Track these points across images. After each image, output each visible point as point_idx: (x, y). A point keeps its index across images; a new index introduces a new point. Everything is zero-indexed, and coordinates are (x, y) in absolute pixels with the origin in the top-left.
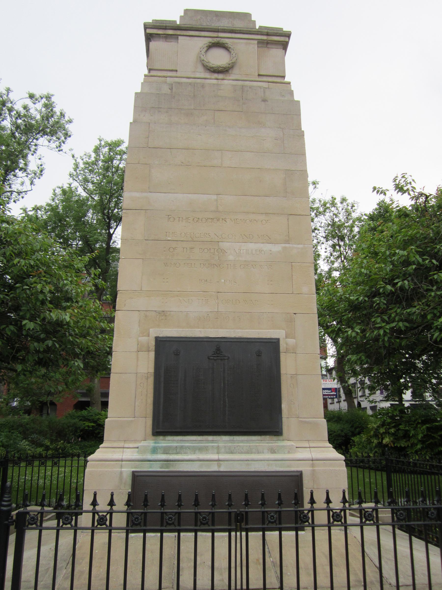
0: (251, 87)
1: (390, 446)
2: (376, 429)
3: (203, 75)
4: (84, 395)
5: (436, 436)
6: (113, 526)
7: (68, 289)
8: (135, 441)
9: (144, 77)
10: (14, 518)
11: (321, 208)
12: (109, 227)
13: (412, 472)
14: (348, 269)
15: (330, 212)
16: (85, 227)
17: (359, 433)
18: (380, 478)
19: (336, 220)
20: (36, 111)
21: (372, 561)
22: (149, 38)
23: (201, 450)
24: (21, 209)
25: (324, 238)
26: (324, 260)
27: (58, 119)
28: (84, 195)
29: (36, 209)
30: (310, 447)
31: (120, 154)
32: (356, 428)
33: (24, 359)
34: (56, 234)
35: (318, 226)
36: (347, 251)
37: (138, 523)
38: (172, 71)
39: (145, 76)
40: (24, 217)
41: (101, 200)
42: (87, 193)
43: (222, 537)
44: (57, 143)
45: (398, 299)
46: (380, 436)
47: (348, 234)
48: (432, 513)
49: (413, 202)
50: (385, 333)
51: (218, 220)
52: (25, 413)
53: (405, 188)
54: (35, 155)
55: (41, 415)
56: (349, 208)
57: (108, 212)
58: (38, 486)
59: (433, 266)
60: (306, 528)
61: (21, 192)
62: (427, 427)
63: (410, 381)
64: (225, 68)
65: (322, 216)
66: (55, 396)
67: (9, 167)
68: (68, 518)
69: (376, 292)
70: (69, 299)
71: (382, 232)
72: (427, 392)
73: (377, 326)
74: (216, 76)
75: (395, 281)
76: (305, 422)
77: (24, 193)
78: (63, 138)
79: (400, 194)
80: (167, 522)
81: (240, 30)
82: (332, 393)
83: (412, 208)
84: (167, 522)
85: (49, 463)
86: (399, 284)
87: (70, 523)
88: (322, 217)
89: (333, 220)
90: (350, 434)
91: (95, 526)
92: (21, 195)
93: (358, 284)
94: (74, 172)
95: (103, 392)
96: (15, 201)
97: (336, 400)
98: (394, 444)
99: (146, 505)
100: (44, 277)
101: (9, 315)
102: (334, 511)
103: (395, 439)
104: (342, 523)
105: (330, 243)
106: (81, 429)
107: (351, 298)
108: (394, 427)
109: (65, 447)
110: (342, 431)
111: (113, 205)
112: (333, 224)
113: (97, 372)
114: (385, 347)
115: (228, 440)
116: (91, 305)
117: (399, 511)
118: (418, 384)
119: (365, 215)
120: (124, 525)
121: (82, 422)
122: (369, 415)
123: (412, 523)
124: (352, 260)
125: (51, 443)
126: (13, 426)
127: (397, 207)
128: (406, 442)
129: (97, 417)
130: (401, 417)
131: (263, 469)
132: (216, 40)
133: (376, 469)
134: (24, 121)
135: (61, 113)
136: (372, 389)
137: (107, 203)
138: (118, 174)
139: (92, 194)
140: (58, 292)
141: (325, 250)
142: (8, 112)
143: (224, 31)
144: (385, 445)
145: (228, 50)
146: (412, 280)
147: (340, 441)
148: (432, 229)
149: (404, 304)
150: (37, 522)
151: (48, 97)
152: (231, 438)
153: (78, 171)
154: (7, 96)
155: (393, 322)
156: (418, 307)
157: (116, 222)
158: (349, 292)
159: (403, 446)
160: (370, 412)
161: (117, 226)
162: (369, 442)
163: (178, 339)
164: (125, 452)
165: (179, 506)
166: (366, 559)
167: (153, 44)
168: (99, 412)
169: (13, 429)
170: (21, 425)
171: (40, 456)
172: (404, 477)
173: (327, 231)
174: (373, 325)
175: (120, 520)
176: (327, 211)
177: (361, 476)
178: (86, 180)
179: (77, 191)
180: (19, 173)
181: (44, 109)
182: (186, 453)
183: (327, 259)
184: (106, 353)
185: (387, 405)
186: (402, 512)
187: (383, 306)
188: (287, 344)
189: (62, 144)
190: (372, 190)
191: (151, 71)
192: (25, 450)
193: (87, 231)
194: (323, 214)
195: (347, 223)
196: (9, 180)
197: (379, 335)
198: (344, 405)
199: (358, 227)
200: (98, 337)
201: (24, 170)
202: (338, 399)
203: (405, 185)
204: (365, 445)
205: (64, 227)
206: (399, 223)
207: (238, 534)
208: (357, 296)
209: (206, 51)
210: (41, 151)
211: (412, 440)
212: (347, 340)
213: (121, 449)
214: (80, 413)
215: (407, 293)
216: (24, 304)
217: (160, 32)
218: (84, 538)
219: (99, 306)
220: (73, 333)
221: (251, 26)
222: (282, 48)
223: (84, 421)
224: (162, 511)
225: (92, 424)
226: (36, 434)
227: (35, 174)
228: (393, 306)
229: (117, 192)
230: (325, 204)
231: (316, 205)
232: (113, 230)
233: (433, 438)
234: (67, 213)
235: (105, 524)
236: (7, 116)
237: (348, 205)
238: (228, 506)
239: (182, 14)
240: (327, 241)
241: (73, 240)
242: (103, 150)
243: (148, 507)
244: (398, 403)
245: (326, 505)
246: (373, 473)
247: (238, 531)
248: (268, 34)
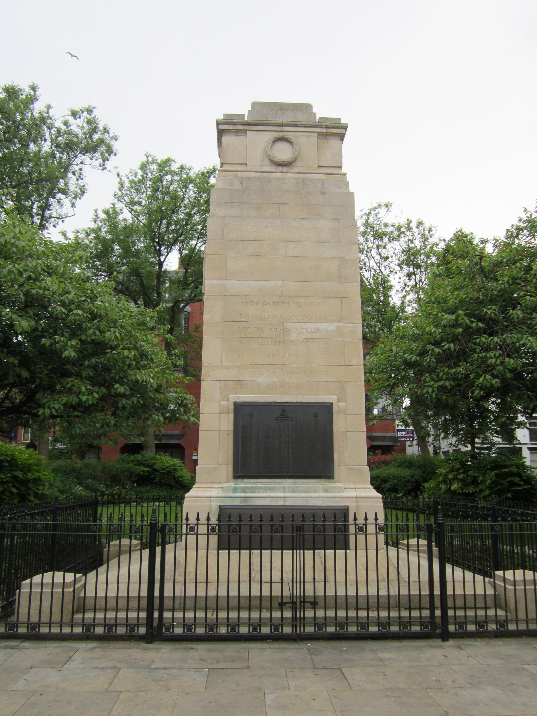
0: (311, 180)
5: (504, 482)
8: (220, 483)
20: (77, 126)
22: (221, 133)
23: (271, 489)
24: (59, 233)
32: (428, 474)
43: (288, 553)
50: (433, 391)
56: (426, 232)
62: (496, 473)
74: (281, 169)
75: (443, 344)
76: (352, 469)
82: (408, 435)
86: (446, 347)
87: (194, 531)
88: (396, 243)
89: (409, 245)
90: (421, 480)
94: (120, 192)
96: (54, 226)
98: (462, 490)
103: (463, 485)
105: (405, 271)
108: (463, 473)
110: (412, 477)
121: (137, 467)
126: (65, 471)
128: (474, 488)
131: (318, 504)
132: (280, 135)
135: (105, 129)
144: (453, 491)
152: (294, 480)
159: (471, 492)
161: (168, 253)
164: (212, 489)
169: (66, 475)
176: (402, 235)
182: (259, 492)
187: (432, 365)
188: (338, 407)
191: (224, 165)
201: (65, 192)
211: (481, 487)
213: (210, 489)
217: (231, 127)
223: (139, 465)
226: (91, 479)
230: (398, 229)
231: (389, 230)
232: (164, 257)
233: (502, 484)
237: (424, 230)
248: (327, 127)
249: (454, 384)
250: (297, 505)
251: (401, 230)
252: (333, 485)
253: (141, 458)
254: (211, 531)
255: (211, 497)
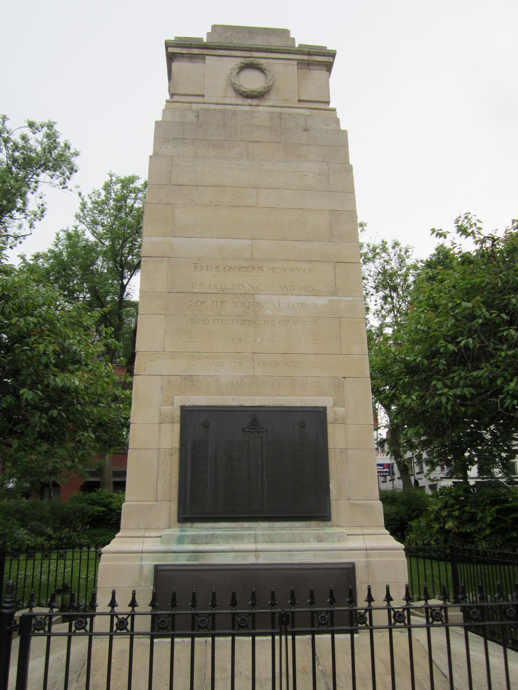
1: (453, 531)
2: (438, 512)
3: (233, 101)
4: (93, 474)
6: (94, 631)
7: (76, 350)
8: (158, 529)
9: (165, 103)
10: (18, 622)
11: (370, 254)
12: (122, 277)
13: (479, 562)
14: (402, 325)
15: (380, 258)
16: (93, 277)
17: (417, 517)
18: (444, 571)
19: (388, 267)
20: (37, 141)
21: (438, 668)
22: (171, 58)
23: (235, 538)
24: (18, 256)
25: (374, 288)
26: (374, 314)
27: (62, 151)
28: (92, 239)
29: (37, 257)
30: (363, 535)
31: (135, 192)
32: (413, 511)
33: (22, 433)
34: (59, 285)
35: (366, 274)
36: (400, 303)
37: (163, 626)
38: (198, 96)
39: (167, 101)
40: (24, 267)
41: (113, 246)
42: (96, 237)
43: (264, 642)
44: (61, 179)
45: (463, 360)
46: (442, 520)
47: (402, 283)
48: (511, 611)
49: (478, 247)
51: (254, 269)
52: (22, 496)
53: (469, 231)
54: (35, 193)
55: (42, 498)
57: (121, 259)
58: (40, 582)
59: (503, 321)
60: (359, 630)
61: (19, 237)
62: (497, 509)
63: (476, 455)
64: (260, 93)
65: (371, 262)
66: (58, 476)
67: (4, 207)
68: (81, 622)
69: (436, 351)
70: (77, 362)
71: (442, 281)
72: (496, 468)
73: (438, 392)
74: (249, 101)
75: (458, 340)
76: (357, 505)
77: (22, 238)
78: (68, 173)
79: (463, 237)
80: (199, 626)
81: (277, 49)
82: (384, 470)
83: (477, 254)
84: (199, 626)
85: (54, 556)
86: (462, 343)
87: (84, 628)
88: (371, 264)
89: (384, 268)
90: (407, 517)
91: (114, 630)
92: (19, 240)
93: (415, 342)
95: (114, 470)
96: (11, 247)
97: (389, 478)
98: (458, 529)
99: (174, 606)
100: (48, 336)
101: (6, 381)
102: (396, 610)
103: (460, 523)
104: (405, 624)
105: (381, 294)
106: (89, 514)
107: (408, 358)
108: (458, 509)
109: (70, 536)
110: (397, 514)
111: (127, 251)
112: (384, 272)
113: (110, 447)
114: (447, 416)
115: (267, 526)
116: (103, 369)
117: (472, 609)
118: (485, 459)
119: (421, 261)
120: (148, 629)
121: (90, 507)
122: (428, 496)
123: (487, 623)
124: (407, 314)
125: (55, 531)
126: (9, 512)
127: (460, 252)
128: (472, 526)
129: (109, 500)
130: (466, 498)
132: (249, 60)
133: (439, 559)
134: (23, 153)
135: (66, 145)
136: (433, 465)
137: (120, 249)
138: (133, 216)
139: (101, 238)
140: (63, 353)
141: (375, 303)
142: (3, 144)
143: (258, 50)
144: (447, 530)
145: (263, 72)
146: (479, 337)
147: (397, 527)
148: (500, 278)
149: (470, 365)
150: (44, 627)
151: (50, 126)
152: (271, 524)
153: (85, 212)
154: (3, 125)
155: (457, 386)
156: (485, 369)
157: (131, 271)
158: (405, 352)
159: (469, 531)
160: (428, 492)
161: (131, 276)
162: (429, 527)
163: (208, 409)
164: (145, 542)
165: (214, 606)
166: (434, 667)
167: (175, 65)
168: (111, 495)
169: (8, 516)
170: (18, 511)
171: (41, 548)
172: (472, 568)
173: (376, 281)
174: (433, 391)
175: (143, 623)
176: (377, 257)
177: (421, 567)
178: (95, 222)
179: (84, 235)
180: (16, 214)
181: (45, 140)
182: (217, 543)
183: (377, 313)
184: (120, 424)
185: (448, 483)
186: (475, 610)
188: (335, 413)
189: (67, 180)
190: (431, 232)
192: (24, 541)
193: (96, 282)
194: (372, 261)
195: (400, 271)
196: (4, 222)
197: (441, 402)
198: (399, 484)
199: (413, 275)
200: (110, 407)
201: (22, 210)
202: (391, 477)
203: (469, 227)
204: (424, 530)
205: (69, 278)
206: (461, 270)
207: (283, 637)
208: (414, 356)
209: (238, 73)
210: (42, 188)
211: (480, 525)
212: (402, 408)
213: (141, 539)
214: (88, 495)
215: (473, 352)
216: (24, 367)
217: (184, 51)
218: (100, 645)
219: (111, 370)
220: (82, 401)
221: (290, 44)
222: (326, 69)
223: (93, 505)
224: (193, 612)
225: (103, 509)
226: (37, 521)
227: (35, 215)
228: (456, 368)
229: (131, 236)
230: (374, 250)
231: (364, 250)
232: (127, 280)
233: (504, 521)
234: (73, 261)
235: (126, 628)
236: (2, 148)
237: (400, 250)
238: (171, 607)
239: (210, 31)
240: (377, 292)
241: (80, 293)
242: (114, 187)
243: (196, 607)
244: (462, 481)
245: (386, 603)
246: (435, 564)
247: (283, 635)
248: (309, 54)
249: (474, 392)
250: (276, 562)
251: (377, 251)
252: (329, 530)
253: (96, 497)
254: (118, 628)
255: (142, 553)
